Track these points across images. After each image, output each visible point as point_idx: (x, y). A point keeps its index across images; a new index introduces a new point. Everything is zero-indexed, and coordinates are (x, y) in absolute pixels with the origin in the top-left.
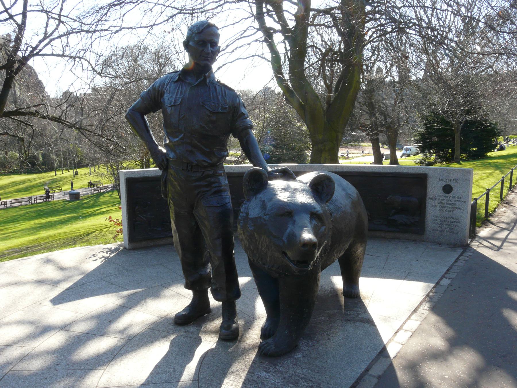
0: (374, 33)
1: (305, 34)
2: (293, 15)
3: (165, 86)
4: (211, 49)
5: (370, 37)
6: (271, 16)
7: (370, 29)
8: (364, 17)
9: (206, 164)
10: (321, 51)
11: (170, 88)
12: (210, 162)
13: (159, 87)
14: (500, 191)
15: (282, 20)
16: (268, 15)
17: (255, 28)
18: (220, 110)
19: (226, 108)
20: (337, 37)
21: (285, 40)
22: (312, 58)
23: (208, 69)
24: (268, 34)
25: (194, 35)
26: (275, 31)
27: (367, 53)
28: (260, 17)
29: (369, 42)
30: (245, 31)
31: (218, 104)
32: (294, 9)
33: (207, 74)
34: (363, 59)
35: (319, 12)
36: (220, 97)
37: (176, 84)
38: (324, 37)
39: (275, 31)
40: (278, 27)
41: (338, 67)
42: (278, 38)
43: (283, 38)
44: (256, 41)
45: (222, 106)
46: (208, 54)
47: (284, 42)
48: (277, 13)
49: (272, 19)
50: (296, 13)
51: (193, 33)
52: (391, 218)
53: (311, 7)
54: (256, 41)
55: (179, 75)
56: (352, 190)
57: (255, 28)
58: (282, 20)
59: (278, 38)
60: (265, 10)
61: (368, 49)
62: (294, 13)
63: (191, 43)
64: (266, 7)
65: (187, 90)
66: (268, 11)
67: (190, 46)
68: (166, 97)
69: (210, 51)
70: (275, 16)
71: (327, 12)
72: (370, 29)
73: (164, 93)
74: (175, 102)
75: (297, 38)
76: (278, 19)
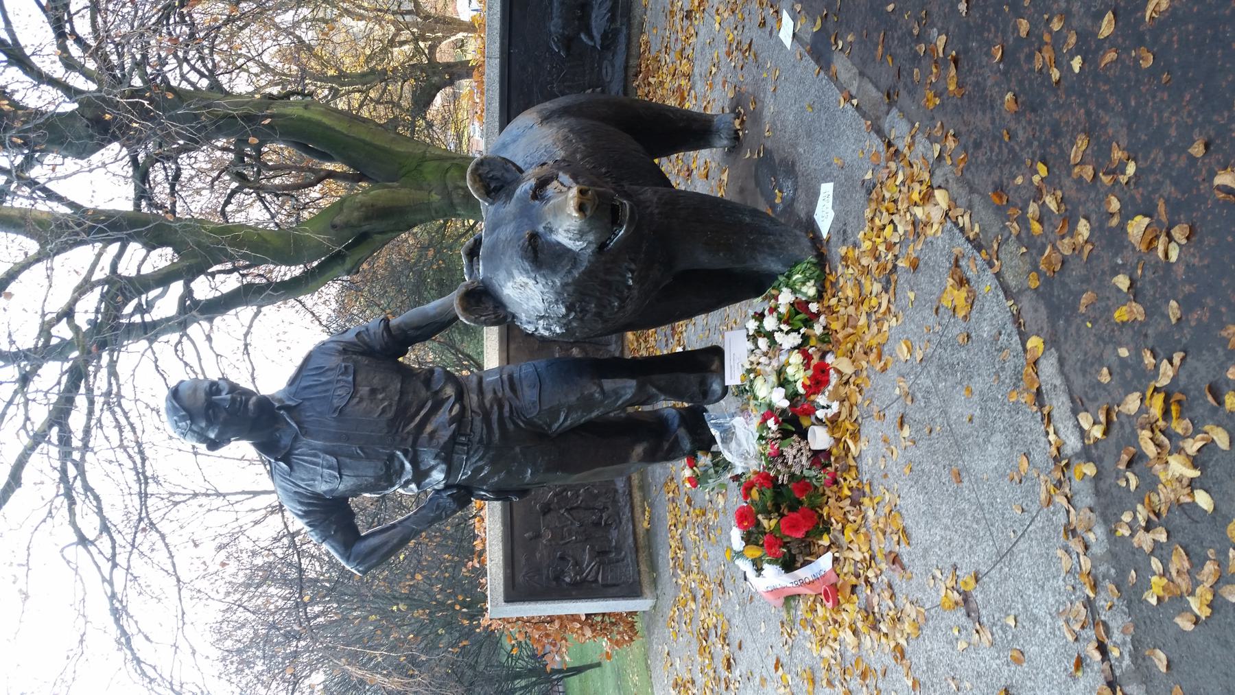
0: (193, 68)
1: (194, 226)
2: (149, 252)
3: (301, 490)
4: (224, 393)
5: (202, 75)
6: (150, 305)
7: (183, 77)
8: (158, 89)
9: (457, 407)
10: (234, 193)
11: (303, 480)
12: (452, 399)
13: (301, 503)
14: (21, 258)
15: (163, 279)
16: (147, 311)
17: (180, 342)
18: (351, 378)
19: (346, 367)
20: (201, 158)
21: (207, 274)
22: (253, 213)
23: (265, 404)
24: (192, 309)
25: (194, 428)
26: (188, 292)
27: (241, 85)
28: (150, 331)
29: (212, 75)
30: (186, 364)
31: (338, 381)
32: (135, 250)
33: (277, 405)
34: (632, 272)
35: (143, 193)
36: (324, 380)
37: (295, 467)
38: (200, 187)
39: (188, 292)
40: (177, 288)
41: (276, 152)
42: (203, 289)
43: (202, 277)
44: (209, 338)
45: (342, 374)
46: (233, 400)
47: (213, 275)
48: (148, 288)
49: (158, 303)
50: (145, 245)
51: (191, 430)
52: (599, 41)
53: (129, 207)
54: (209, 338)
55: (277, 460)
56: (527, 119)
57: (180, 342)
58: (163, 279)
59: (203, 289)
60: (137, 319)
61: (231, 80)
62: (144, 251)
63: (212, 436)
64: (132, 315)
65: (306, 445)
66: (139, 309)
67: (217, 436)
68: (322, 487)
69: (229, 396)
70: (153, 294)
71: (141, 175)
72: (183, 77)
73: (313, 493)
74: (330, 467)
75: (200, 248)
76: (158, 286)
